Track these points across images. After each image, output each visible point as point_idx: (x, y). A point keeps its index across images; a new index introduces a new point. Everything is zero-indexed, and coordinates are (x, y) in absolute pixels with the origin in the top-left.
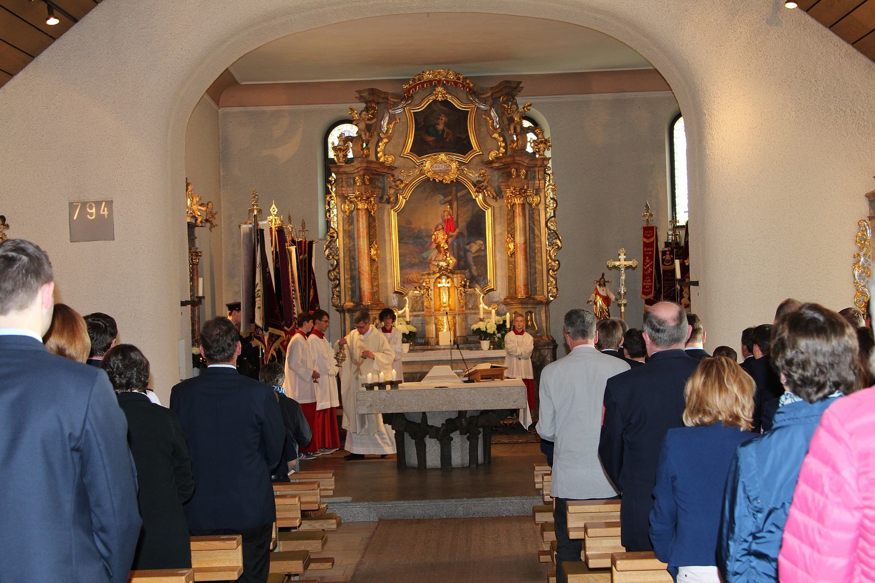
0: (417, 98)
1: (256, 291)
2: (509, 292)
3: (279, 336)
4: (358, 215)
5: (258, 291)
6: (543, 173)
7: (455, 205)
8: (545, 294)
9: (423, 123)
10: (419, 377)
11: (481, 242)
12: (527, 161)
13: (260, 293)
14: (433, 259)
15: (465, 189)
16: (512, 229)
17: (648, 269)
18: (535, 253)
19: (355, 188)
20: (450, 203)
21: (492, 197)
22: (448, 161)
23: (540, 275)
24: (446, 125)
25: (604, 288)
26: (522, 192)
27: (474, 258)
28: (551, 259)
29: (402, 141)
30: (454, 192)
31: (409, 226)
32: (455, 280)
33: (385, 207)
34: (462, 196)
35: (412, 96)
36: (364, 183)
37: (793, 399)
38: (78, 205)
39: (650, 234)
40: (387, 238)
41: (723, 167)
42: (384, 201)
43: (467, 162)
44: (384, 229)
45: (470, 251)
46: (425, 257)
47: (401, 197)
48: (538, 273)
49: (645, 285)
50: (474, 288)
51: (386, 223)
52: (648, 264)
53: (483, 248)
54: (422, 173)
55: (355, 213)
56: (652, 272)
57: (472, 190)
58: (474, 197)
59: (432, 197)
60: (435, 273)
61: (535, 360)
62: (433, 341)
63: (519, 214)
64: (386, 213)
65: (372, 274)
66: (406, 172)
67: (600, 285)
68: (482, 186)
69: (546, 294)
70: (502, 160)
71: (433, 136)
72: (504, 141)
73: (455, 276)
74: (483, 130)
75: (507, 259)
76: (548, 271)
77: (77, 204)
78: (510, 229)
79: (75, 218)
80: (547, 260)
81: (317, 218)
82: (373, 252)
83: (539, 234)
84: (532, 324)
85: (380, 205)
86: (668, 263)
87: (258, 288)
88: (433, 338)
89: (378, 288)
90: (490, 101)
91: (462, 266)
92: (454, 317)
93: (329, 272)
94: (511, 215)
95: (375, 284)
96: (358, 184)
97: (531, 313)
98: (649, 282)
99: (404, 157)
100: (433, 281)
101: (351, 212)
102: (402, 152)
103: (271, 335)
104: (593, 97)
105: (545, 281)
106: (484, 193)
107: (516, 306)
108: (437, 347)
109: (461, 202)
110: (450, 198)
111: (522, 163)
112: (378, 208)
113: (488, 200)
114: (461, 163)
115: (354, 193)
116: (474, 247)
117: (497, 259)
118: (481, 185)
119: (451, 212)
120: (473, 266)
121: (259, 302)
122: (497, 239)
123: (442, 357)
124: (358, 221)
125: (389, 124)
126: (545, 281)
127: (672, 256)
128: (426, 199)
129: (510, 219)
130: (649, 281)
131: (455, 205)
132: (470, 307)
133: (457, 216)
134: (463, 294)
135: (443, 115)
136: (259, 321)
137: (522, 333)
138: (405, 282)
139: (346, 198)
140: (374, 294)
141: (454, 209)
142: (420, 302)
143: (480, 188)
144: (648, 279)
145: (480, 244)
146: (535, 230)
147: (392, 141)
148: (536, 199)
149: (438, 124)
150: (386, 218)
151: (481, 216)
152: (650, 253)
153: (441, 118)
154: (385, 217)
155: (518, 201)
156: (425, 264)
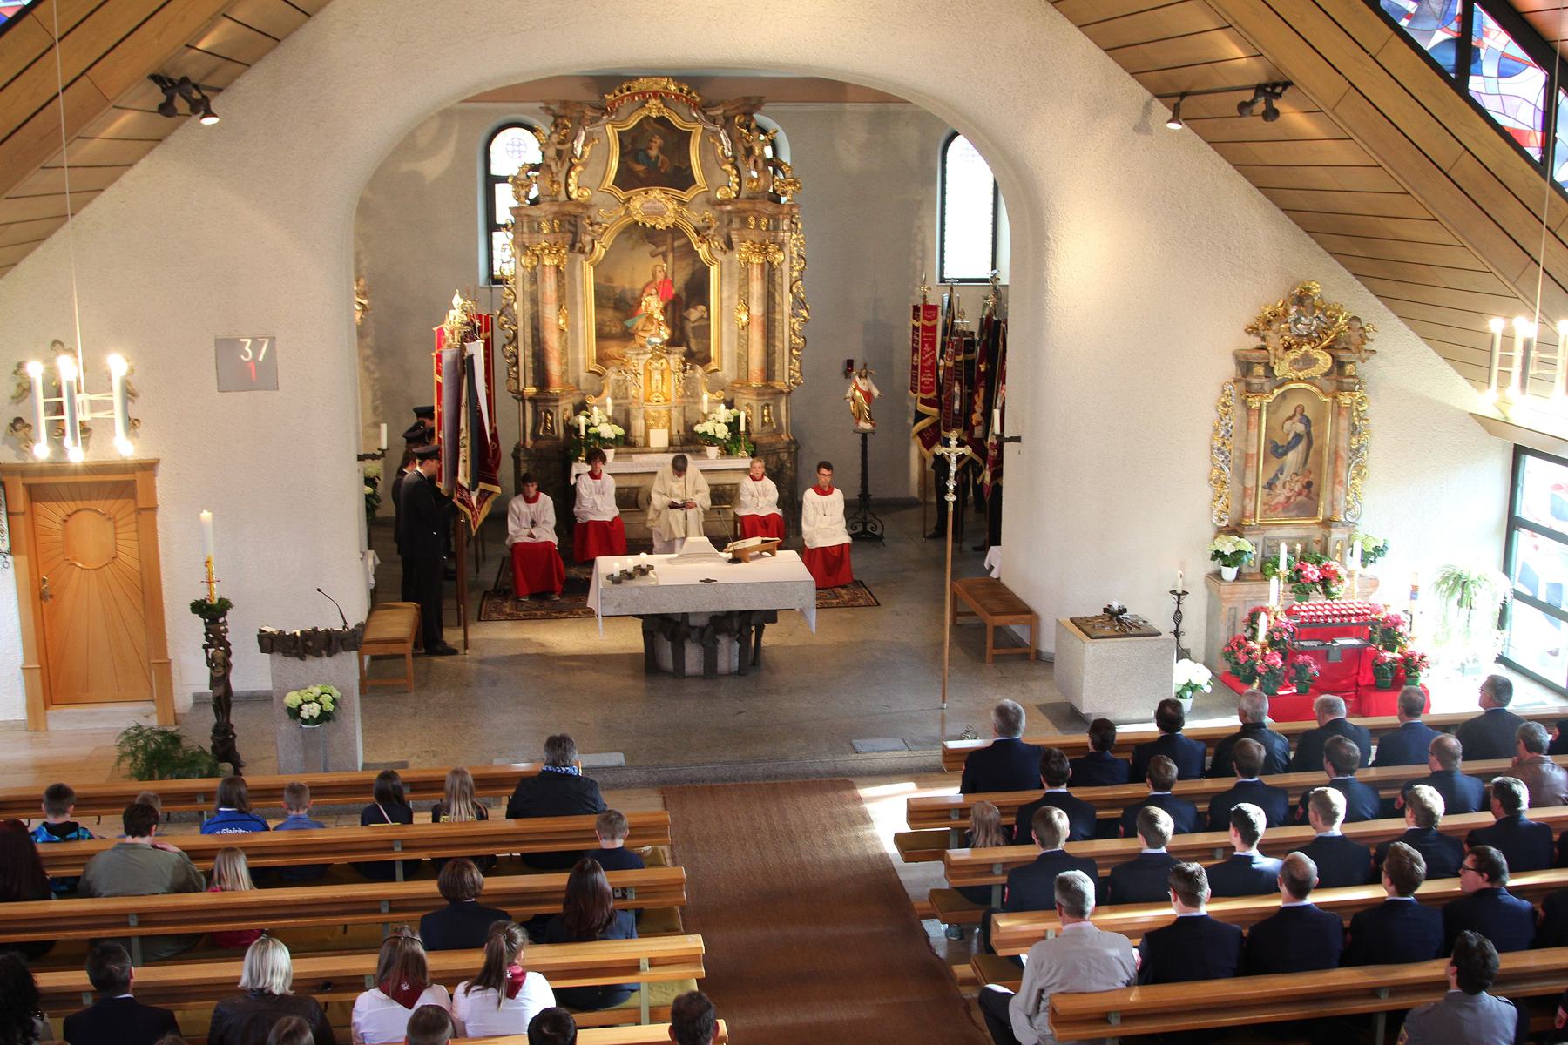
0: (623, 112)
2: (739, 374)
3: (491, 493)
4: (544, 273)
9: (630, 146)
11: (703, 308)
13: (467, 442)
17: (928, 359)
20: (664, 255)
24: (661, 150)
26: (763, 249)
27: (693, 328)
28: (795, 334)
29: (601, 169)
32: (672, 362)
34: (679, 247)
35: (617, 110)
36: (553, 231)
40: (579, 299)
51: (578, 279)
52: (927, 353)
53: (706, 316)
54: (628, 213)
55: (539, 268)
58: (695, 248)
62: (640, 441)
64: (578, 266)
67: (860, 377)
69: (787, 380)
72: (739, 175)
74: (710, 158)
79: (261, 359)
81: (477, 258)
82: (561, 321)
85: (571, 255)
87: (463, 435)
90: (722, 121)
92: (670, 411)
93: (504, 346)
96: (545, 231)
97: (768, 405)
100: (642, 363)
101: (534, 268)
104: (848, 106)
105: (787, 364)
108: (647, 449)
112: (569, 260)
113: (713, 252)
116: (694, 314)
117: (724, 329)
121: (464, 453)
124: (544, 280)
125: (584, 145)
126: (787, 364)
128: (633, 248)
131: (670, 257)
136: (463, 479)
138: (602, 359)
139: (527, 248)
140: (564, 373)
143: (704, 237)
147: (588, 169)
148: (780, 257)
150: (578, 272)
155: (755, 260)
156: (628, 336)
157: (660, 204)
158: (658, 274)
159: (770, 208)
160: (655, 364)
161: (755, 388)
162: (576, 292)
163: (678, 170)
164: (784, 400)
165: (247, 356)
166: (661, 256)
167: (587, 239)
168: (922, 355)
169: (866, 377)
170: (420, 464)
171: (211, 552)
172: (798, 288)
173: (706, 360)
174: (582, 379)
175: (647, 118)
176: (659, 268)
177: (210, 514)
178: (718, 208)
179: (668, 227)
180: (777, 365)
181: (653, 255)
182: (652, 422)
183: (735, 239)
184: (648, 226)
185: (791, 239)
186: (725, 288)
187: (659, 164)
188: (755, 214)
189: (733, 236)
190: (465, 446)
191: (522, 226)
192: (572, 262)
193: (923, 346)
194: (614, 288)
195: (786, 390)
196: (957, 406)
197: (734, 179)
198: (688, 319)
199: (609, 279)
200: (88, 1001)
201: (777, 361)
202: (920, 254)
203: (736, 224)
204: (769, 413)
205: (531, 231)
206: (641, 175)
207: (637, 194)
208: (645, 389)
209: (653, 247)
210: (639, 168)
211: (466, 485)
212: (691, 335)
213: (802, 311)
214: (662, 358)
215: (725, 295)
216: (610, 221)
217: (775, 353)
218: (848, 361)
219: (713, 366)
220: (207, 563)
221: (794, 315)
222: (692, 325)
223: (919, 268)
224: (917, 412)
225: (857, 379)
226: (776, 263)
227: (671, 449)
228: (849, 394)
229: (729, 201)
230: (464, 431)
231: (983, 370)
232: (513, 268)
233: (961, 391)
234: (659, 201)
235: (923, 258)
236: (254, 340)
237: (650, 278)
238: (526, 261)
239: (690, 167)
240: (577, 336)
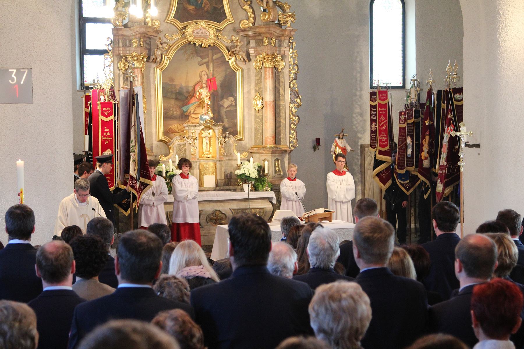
1: (131, 146)
5: (133, 146)
6: (288, 42)
8: (287, 144)
11: (232, 99)
12: (278, 32)
14: (192, 112)
15: (220, 52)
16: (259, 88)
18: (280, 109)
19: (131, 49)
21: (243, 60)
22: (207, 28)
23: (284, 128)
25: (342, 141)
26: (273, 58)
27: (226, 112)
30: (210, 55)
31: (172, 83)
32: (216, 131)
33: (151, 65)
38: (25, 72)
39: (384, 96)
40: (153, 93)
41: (515, 57)
42: (151, 60)
43: (221, 29)
44: (150, 85)
45: (223, 107)
47: (166, 57)
48: (282, 126)
49: (381, 139)
51: (152, 80)
52: (382, 122)
53: (234, 104)
56: (386, 128)
57: (225, 52)
58: (227, 60)
59: (192, 58)
60: (201, 126)
63: (269, 77)
64: (152, 71)
66: (169, 35)
67: (339, 138)
68: (236, 51)
69: (288, 144)
70: (255, 30)
71: (193, 5)
73: (217, 128)
76: (290, 125)
77: (24, 70)
78: (258, 89)
79: (22, 83)
80: (290, 116)
83: (284, 94)
84: (279, 170)
86: (402, 122)
87: (132, 144)
91: (217, 119)
92: (216, 164)
94: (259, 76)
96: (134, 45)
97: (278, 160)
98: (385, 137)
99: (168, 23)
100: (198, 132)
102: (166, 18)
103: (142, 184)
105: (288, 134)
106: (235, 56)
107: (266, 154)
109: (216, 64)
111: (274, 33)
113: (238, 63)
114: (218, 30)
115: (131, 54)
116: (226, 103)
117: (245, 113)
118: (235, 50)
119: (207, 72)
120: (225, 119)
122: (245, 97)
123: (214, 197)
126: (288, 134)
127: (405, 117)
128: (187, 60)
129: (258, 79)
130: (384, 135)
134: (224, 144)
137: (294, 179)
138: (168, 132)
142: (184, 149)
143: (233, 52)
144: (383, 134)
146: (280, 90)
148: (282, 64)
150: (151, 75)
151: (234, 75)
152: (384, 113)
154: (151, 74)
155: (268, 65)
157: (205, 31)
158: (203, 76)
159: (278, 31)
160: (205, 134)
161: (270, 148)
162: (150, 88)
163: (215, 9)
164: (286, 157)
165: (13, 80)
166: (205, 65)
167: (159, 52)
168: (379, 123)
169: (342, 138)
170: (100, 166)
171: (22, 186)
172: (294, 84)
173: (235, 133)
174: (154, 146)
177: (22, 162)
178: (241, 33)
179: (209, 46)
180: (282, 135)
182: (205, 171)
183: (252, 52)
184: (197, 45)
185: (289, 52)
186: (246, 86)
187: (203, 6)
188: (268, 35)
189: (251, 52)
190: (134, 151)
191: (118, 43)
192: (148, 68)
193: (379, 118)
194: (175, 86)
195: (289, 150)
196: (409, 152)
197: (251, 15)
198: (222, 106)
199: (172, 80)
201: (281, 132)
202: (359, 70)
203: (253, 43)
204: (278, 164)
205: (125, 45)
206: (192, 12)
207: (190, 24)
208: (199, 149)
210: (191, 7)
211: (135, 176)
212: (225, 117)
213: (296, 99)
214: (210, 128)
215: (246, 90)
216: (172, 42)
217: (280, 126)
218: (316, 139)
219: (240, 136)
220: (20, 194)
221: (292, 102)
222: (225, 110)
223: (359, 78)
224: (375, 160)
225: (337, 139)
226: (280, 68)
227: (218, 188)
228: (332, 149)
229: (250, 28)
230: (134, 142)
231: (427, 124)
232: (112, 70)
233: (413, 142)
234: (204, 28)
235: (361, 73)
236: (18, 70)
238: (121, 65)
239: (223, 7)
240: (151, 118)
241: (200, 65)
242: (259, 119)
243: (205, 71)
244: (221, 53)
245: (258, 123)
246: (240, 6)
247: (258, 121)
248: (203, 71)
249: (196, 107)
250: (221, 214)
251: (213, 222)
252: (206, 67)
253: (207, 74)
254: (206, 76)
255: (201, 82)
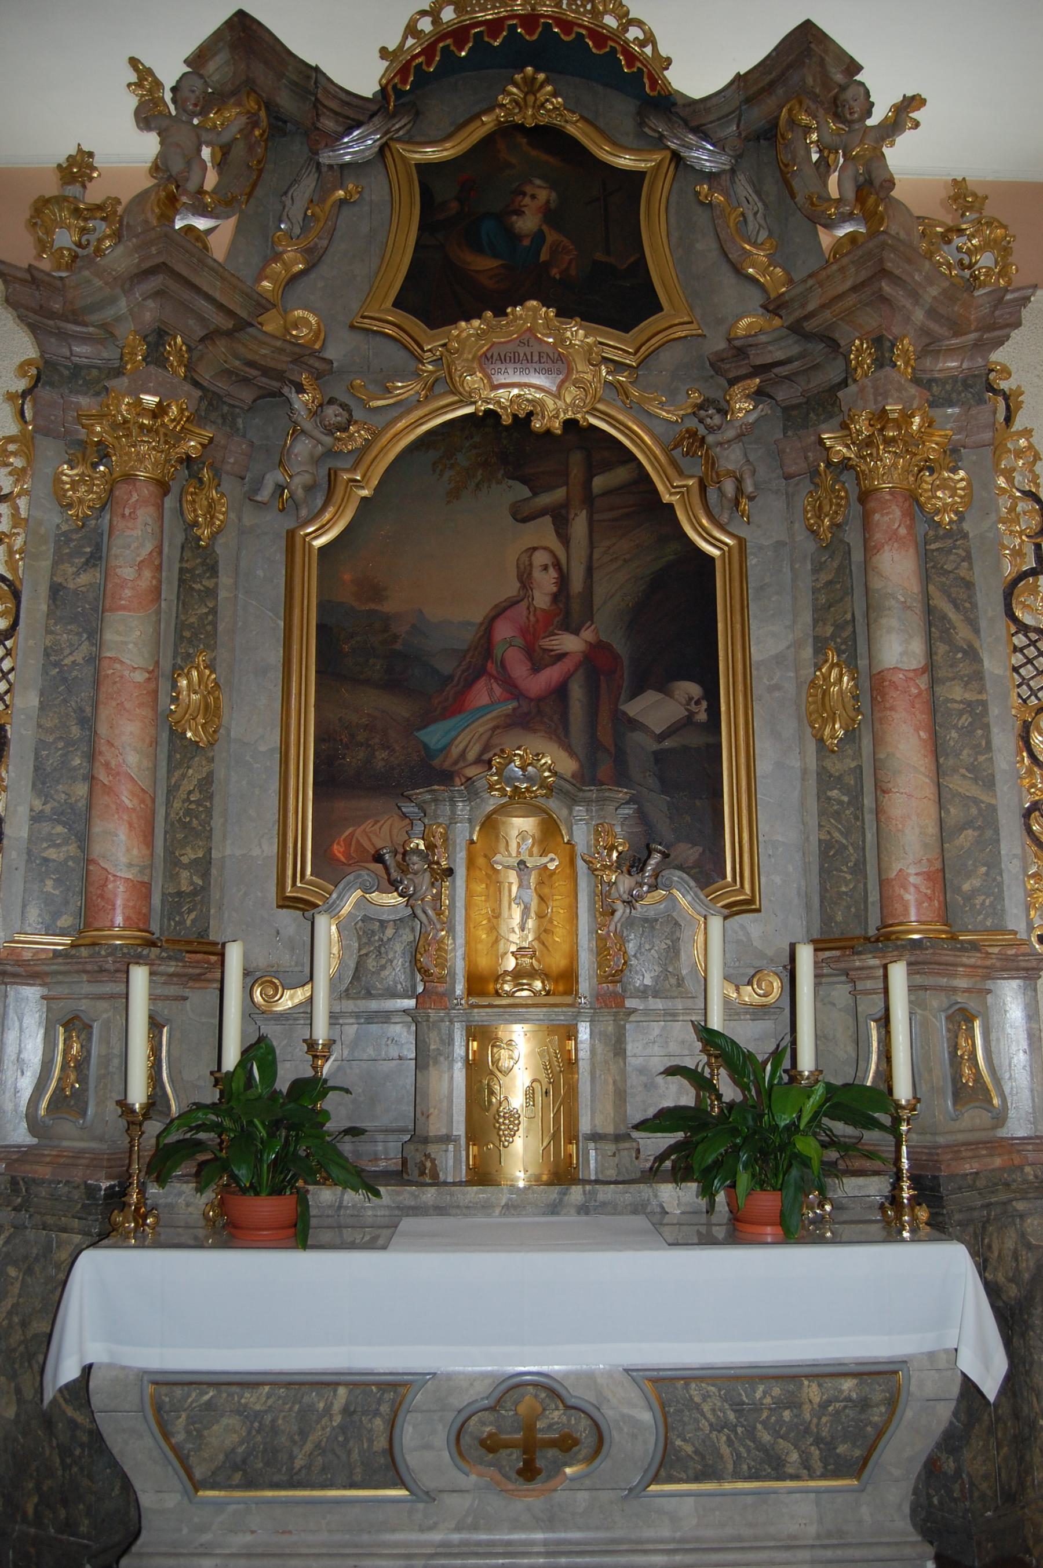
7: (579, 525)
9: (454, 206)
10: (346, 1411)
11: (693, 689)
15: (624, 463)
16: (839, 627)
24: (551, 216)
31: (373, 606)
34: (607, 493)
37: (59, 802)
46: (432, 746)
50: (668, 887)
53: (702, 717)
59: (478, 486)
61: (1001, 1278)
65: (177, 804)
71: (495, 255)
73: (579, 810)
75: (812, 764)
78: (829, 630)
88: (447, 1139)
89: (206, 875)
95: (189, 855)
108: (473, 1193)
110: (559, 494)
128: (454, 494)
129: (830, 583)
131: (579, 525)
132: (648, 981)
133: (590, 571)
135: (538, 182)
141: (573, 544)
145: (691, 699)
149: (519, 213)
153: (529, 189)
158: (537, 574)
166: (547, 519)
175: (508, 131)
176: (541, 558)
181: (522, 516)
187: (544, 256)
199: (373, 590)
200: (554, 195)
209: (526, 493)
210: (483, 264)
237: (512, 588)
241: (524, 520)
242: (845, 789)
243: (545, 549)
244: (634, 465)
245: (837, 812)
246: (725, 268)
247: (840, 802)
248: (535, 549)
249: (494, 729)
250: (556, 1415)
251: (500, 1469)
252: (551, 528)
253: (557, 565)
254: (553, 573)
255: (525, 603)
